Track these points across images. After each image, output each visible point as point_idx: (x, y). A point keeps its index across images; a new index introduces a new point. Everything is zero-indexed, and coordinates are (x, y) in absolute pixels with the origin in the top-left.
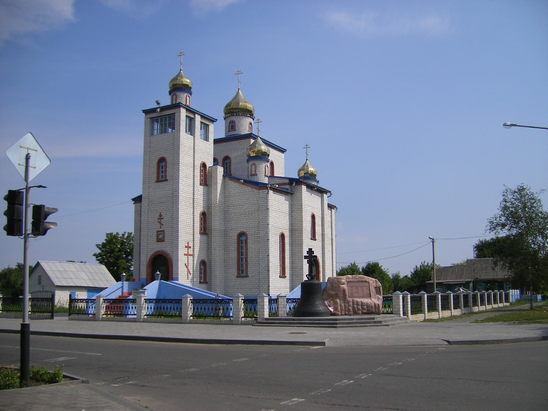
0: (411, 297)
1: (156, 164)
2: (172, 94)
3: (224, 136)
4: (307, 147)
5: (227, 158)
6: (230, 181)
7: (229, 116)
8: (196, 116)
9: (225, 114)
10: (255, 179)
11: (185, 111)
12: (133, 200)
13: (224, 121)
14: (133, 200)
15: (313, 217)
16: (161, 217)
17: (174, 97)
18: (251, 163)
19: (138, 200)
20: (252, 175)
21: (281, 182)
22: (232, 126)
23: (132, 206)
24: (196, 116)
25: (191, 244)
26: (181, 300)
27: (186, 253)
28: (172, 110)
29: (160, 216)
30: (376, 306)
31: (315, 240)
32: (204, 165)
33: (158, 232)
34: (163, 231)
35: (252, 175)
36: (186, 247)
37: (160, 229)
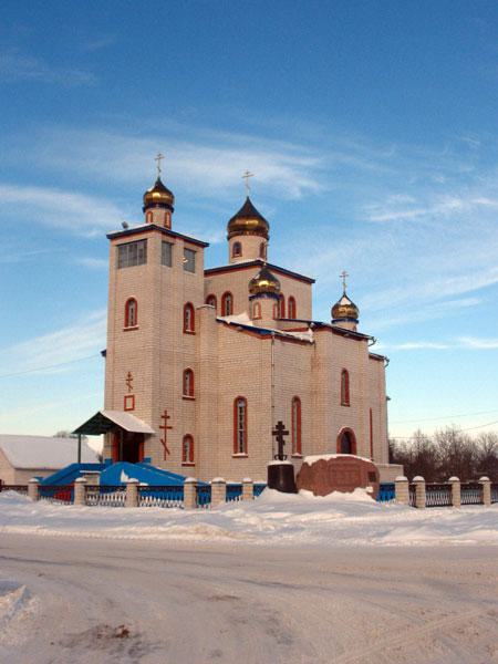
16: (130, 378)
33: (260, 318)
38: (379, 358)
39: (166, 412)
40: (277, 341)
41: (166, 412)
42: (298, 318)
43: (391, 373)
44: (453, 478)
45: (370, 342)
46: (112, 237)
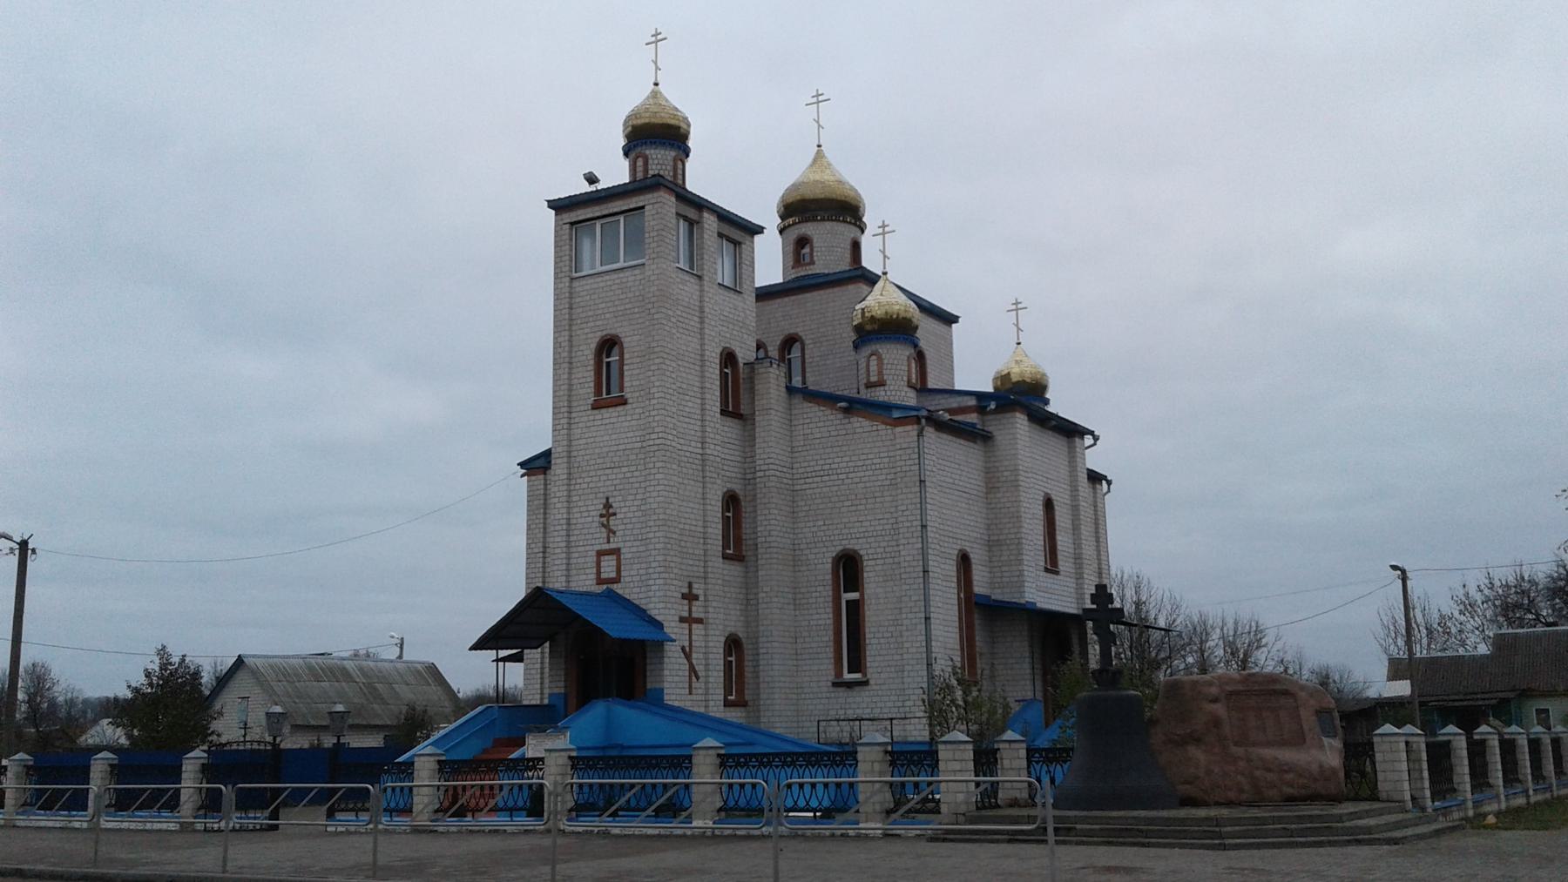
0: (1427, 745)
1: (591, 357)
2: (632, 155)
3: (780, 280)
4: (1017, 307)
5: (790, 342)
6: (806, 404)
7: (794, 223)
8: (706, 215)
9: (783, 218)
10: (881, 395)
11: (673, 199)
12: (522, 465)
13: (779, 239)
14: (522, 465)
15: (1049, 504)
16: (608, 511)
17: (640, 162)
18: (866, 351)
19: (536, 466)
20: (869, 385)
21: (955, 405)
22: (799, 249)
23: (520, 485)
24: (706, 215)
25: (698, 589)
26: (690, 757)
27: (686, 614)
28: (635, 199)
29: (608, 506)
30: (1325, 774)
31: (1057, 573)
32: (728, 358)
33: (600, 554)
34: (616, 552)
35: (869, 385)
36: (684, 596)
37: (606, 547)
38: (1095, 478)
39: (690, 585)
40: (930, 432)
41: (690, 585)
42: (931, 384)
43: (1113, 503)
44: (1484, 728)
45: (1088, 440)
46: (559, 206)
